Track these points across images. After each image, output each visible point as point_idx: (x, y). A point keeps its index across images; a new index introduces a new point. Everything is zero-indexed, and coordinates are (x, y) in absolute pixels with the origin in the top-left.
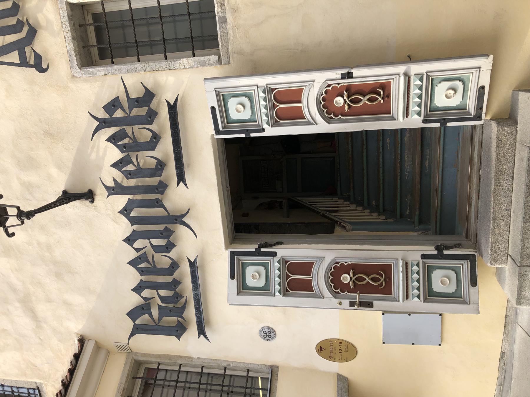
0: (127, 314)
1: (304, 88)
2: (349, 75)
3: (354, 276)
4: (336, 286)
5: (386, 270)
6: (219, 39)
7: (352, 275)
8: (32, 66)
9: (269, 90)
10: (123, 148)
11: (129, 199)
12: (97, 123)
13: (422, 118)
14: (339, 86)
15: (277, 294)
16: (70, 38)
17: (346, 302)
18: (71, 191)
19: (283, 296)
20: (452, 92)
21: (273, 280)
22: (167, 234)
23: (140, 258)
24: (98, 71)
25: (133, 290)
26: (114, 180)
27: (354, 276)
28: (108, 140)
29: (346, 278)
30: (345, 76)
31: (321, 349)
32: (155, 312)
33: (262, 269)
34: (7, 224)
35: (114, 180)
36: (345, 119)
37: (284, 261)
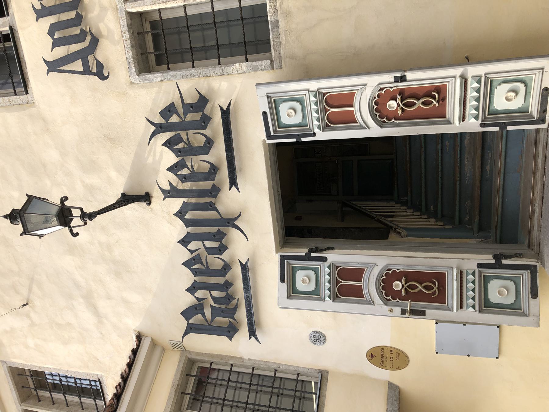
0: (181, 314)
1: (356, 91)
2: (402, 79)
3: (406, 284)
4: (387, 292)
5: (439, 279)
6: (272, 44)
7: (404, 282)
8: (94, 74)
9: (320, 95)
10: (178, 153)
11: (184, 202)
12: (153, 128)
13: (480, 121)
14: (392, 90)
15: (327, 299)
16: (129, 46)
17: (398, 310)
18: (130, 193)
19: (333, 301)
20: (513, 94)
21: (323, 285)
22: (220, 236)
23: (193, 259)
24: (155, 77)
25: (188, 290)
26: (170, 183)
27: (406, 284)
28: (164, 144)
29: (398, 285)
30: (397, 80)
31: (372, 356)
32: (208, 313)
33: (312, 274)
34: (72, 224)
35: (170, 183)
36: (398, 123)
37: (334, 267)
